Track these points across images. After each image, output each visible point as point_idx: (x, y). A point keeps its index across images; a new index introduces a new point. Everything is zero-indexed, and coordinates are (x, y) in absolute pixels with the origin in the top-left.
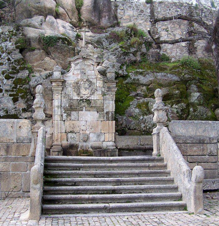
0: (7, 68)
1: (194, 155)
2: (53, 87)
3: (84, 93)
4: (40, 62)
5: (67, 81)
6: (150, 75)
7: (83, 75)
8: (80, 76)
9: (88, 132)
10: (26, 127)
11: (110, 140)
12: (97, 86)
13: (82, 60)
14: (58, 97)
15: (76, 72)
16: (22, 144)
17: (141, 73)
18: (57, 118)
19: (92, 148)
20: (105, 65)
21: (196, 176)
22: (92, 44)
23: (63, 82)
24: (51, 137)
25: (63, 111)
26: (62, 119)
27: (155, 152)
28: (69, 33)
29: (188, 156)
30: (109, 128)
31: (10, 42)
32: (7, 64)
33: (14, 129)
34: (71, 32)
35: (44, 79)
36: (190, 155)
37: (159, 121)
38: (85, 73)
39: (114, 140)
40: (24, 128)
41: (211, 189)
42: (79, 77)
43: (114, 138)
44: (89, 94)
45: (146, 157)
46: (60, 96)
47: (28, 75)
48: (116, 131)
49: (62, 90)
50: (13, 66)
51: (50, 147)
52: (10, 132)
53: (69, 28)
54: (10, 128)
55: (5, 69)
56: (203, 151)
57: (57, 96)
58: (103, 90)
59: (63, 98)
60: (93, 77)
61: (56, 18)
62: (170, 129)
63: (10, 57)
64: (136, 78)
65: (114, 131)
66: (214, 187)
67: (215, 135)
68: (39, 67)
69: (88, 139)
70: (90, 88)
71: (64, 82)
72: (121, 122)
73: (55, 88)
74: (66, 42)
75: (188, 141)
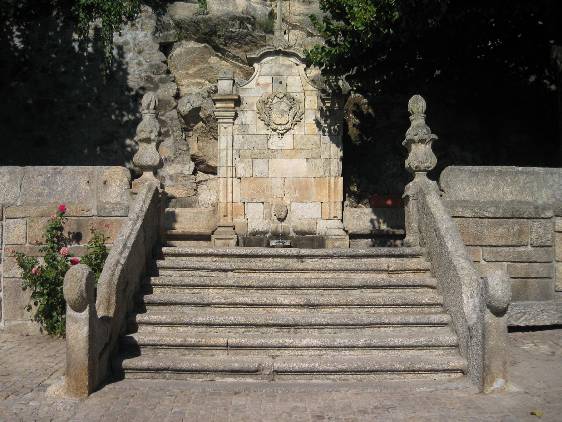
0: (136, 80)
2: (215, 111)
4: (201, 66)
5: (245, 99)
7: (277, 84)
8: (271, 87)
9: (287, 201)
10: (118, 183)
11: (332, 216)
12: (307, 106)
14: (226, 130)
16: (108, 218)
19: (295, 232)
22: (302, 29)
28: (255, 9)
30: (329, 192)
31: (143, 30)
32: (136, 73)
33: (92, 187)
35: (205, 98)
39: (340, 217)
40: (114, 185)
41: (537, 324)
42: (270, 90)
46: (230, 129)
54: (84, 186)
56: (520, 235)
57: (225, 128)
59: (236, 132)
63: (142, 59)
66: (544, 321)
67: (548, 199)
71: (238, 102)
74: (249, 26)
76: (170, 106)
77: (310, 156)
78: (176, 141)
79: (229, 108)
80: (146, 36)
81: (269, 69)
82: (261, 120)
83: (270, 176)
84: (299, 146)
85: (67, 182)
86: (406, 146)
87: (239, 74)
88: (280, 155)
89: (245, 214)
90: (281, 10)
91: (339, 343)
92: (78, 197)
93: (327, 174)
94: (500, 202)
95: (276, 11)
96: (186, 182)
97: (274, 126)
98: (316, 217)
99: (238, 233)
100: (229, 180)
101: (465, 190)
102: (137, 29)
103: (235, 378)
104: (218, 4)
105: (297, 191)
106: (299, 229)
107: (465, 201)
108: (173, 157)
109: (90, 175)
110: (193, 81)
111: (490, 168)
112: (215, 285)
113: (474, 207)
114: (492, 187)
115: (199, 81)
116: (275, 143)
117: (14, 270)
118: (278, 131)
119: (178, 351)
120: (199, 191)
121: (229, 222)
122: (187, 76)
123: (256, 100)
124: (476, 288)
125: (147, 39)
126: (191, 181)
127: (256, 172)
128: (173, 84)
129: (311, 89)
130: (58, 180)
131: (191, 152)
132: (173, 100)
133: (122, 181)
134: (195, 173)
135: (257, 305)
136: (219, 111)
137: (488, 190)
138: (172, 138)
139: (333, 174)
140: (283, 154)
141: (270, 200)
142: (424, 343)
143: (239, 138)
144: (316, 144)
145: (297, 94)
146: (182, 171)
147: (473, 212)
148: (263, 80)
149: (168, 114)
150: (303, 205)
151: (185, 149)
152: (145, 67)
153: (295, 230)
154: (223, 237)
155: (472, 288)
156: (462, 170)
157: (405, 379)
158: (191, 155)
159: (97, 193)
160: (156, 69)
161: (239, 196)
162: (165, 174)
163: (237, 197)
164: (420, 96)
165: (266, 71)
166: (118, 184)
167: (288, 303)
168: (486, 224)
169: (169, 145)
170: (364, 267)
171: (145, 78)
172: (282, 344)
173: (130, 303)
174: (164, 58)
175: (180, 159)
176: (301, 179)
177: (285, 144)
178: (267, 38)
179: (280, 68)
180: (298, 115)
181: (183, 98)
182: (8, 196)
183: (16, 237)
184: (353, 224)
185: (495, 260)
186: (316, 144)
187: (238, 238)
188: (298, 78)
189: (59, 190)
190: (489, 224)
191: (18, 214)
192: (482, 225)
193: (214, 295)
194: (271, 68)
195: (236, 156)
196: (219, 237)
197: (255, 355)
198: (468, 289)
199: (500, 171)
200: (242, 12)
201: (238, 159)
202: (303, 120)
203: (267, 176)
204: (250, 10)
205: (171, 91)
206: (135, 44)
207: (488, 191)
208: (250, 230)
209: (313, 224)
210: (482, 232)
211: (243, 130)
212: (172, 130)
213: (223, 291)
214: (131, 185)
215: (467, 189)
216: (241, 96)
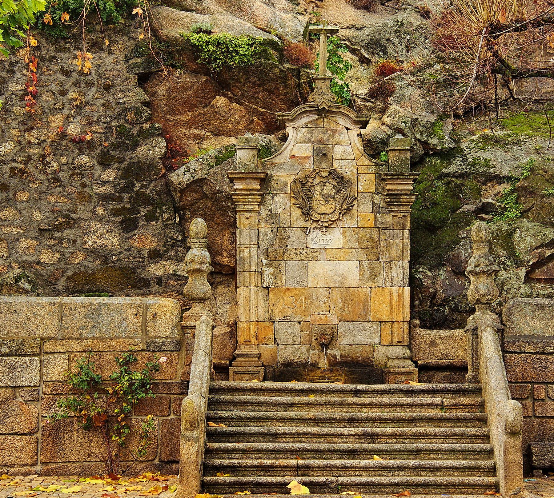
0: (102, 131)
3: (322, 209)
4: (200, 110)
6: (523, 147)
8: (311, 161)
11: (395, 340)
12: (360, 188)
17: (500, 143)
20: (389, 119)
21: (506, 421)
23: (262, 180)
24: (231, 332)
25: (265, 262)
26: (262, 283)
27: (469, 374)
31: (111, 53)
34: (288, 17)
37: (478, 300)
38: (325, 155)
40: (164, 318)
42: (309, 165)
43: (406, 336)
44: (337, 212)
47: (163, 151)
50: (119, 126)
51: (228, 362)
55: (225, 476)
59: (263, 225)
63: (110, 99)
64: (482, 155)
68: (198, 127)
72: (432, 290)
73: (241, 198)
75: (549, 348)
78: (165, 226)
79: (253, 190)
80: (116, 63)
82: (297, 207)
83: (309, 285)
85: (113, 315)
87: (259, 124)
88: (323, 257)
89: (275, 339)
97: (315, 217)
99: (265, 364)
102: (102, 50)
109: (138, 307)
110: (187, 132)
112: (278, 418)
115: (197, 131)
117: (54, 408)
123: (289, 180)
128: (161, 139)
129: (366, 164)
130: (103, 313)
135: (319, 435)
136: (239, 194)
139: (397, 282)
142: (466, 465)
143: (266, 232)
151: (180, 238)
171: (116, 130)
177: (330, 241)
179: (323, 133)
180: (349, 200)
182: (48, 330)
183: (57, 373)
189: (105, 322)
191: (59, 349)
192: (547, 360)
193: (275, 428)
194: (311, 132)
196: (240, 369)
202: (355, 207)
203: (306, 285)
206: (99, 74)
208: (281, 360)
211: (272, 221)
214: (181, 317)
215: (531, 323)
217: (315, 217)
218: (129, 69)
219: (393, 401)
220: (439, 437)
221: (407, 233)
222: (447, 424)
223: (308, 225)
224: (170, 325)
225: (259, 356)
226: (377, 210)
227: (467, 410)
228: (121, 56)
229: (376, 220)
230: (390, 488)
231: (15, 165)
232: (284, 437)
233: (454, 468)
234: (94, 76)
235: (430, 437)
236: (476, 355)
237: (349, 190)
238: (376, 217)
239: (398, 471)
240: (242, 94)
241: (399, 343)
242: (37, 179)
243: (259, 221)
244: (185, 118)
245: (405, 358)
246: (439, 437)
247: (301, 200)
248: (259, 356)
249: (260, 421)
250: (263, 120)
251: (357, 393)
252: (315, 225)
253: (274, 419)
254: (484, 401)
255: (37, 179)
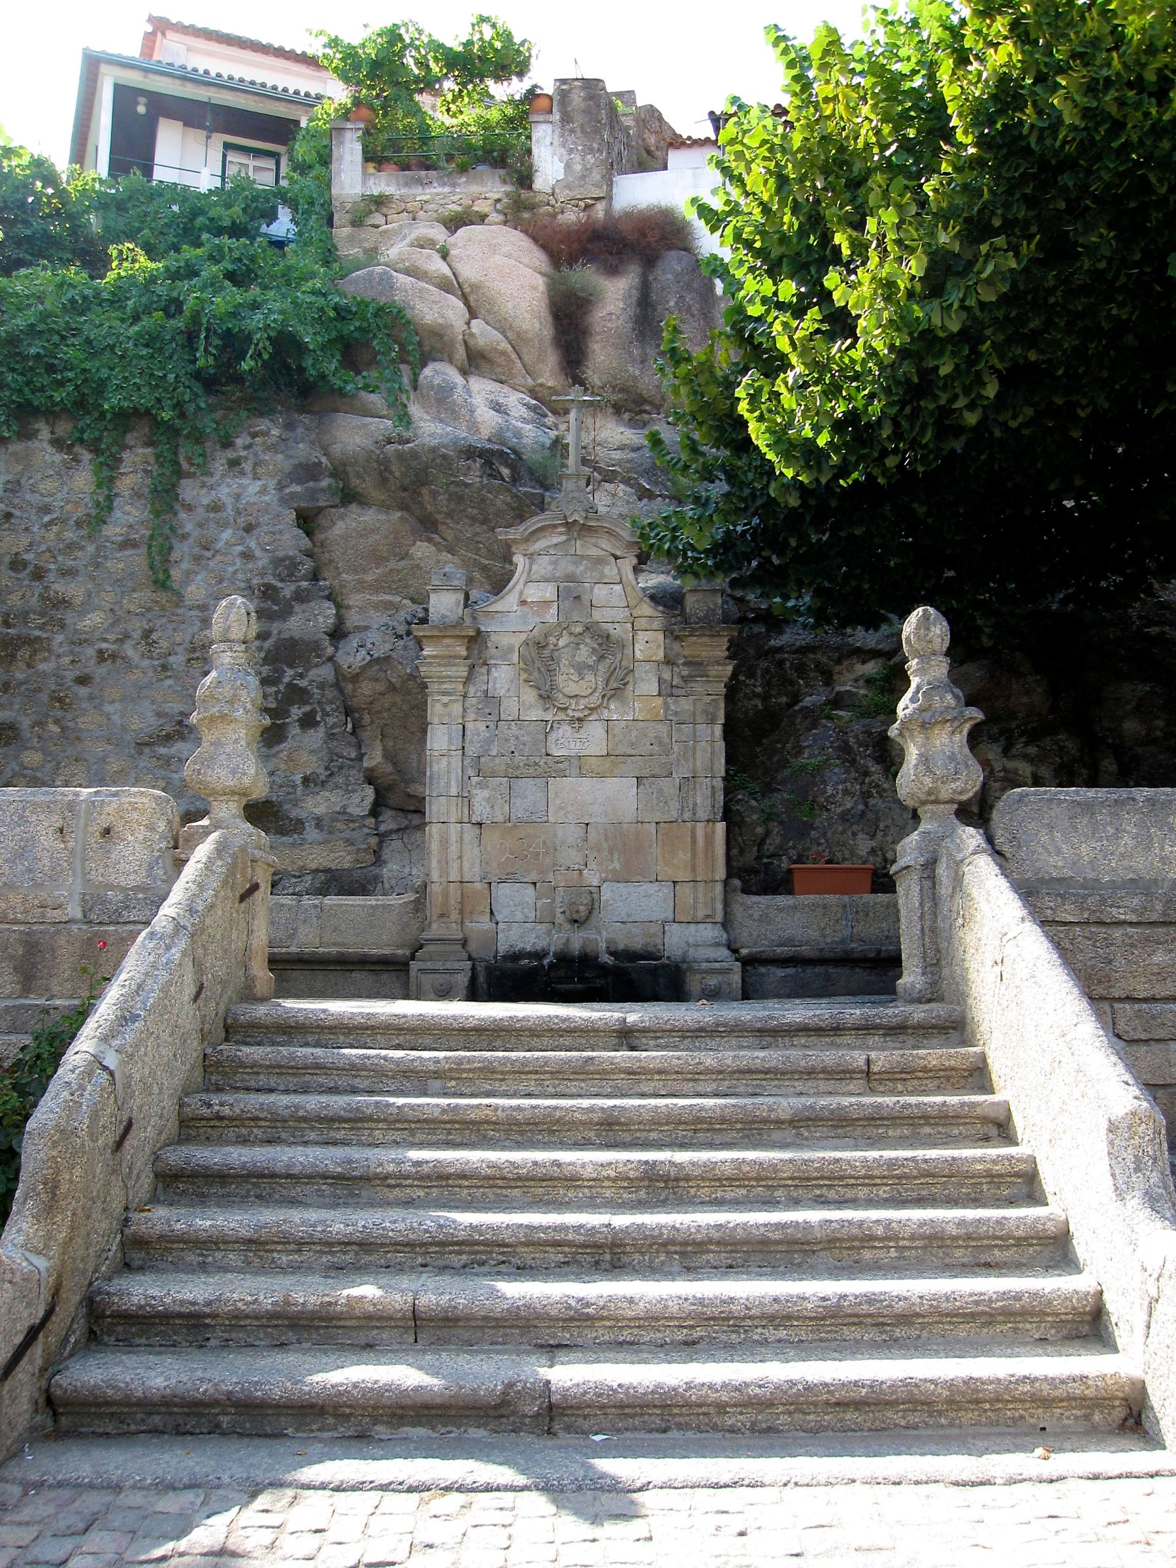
1: (1154, 999)
3: (572, 689)
4: (392, 564)
5: (494, 638)
7: (567, 604)
8: (553, 610)
11: (700, 914)
12: (638, 655)
13: (564, 538)
15: (534, 593)
18: (443, 809)
19: (611, 954)
22: (627, 481)
27: (911, 977)
28: (518, 434)
29: (1120, 1000)
30: (694, 857)
31: (256, 477)
32: (240, 576)
33: (71, 844)
35: (400, 637)
36: (1128, 999)
38: (578, 598)
39: (719, 917)
40: (130, 838)
43: (719, 906)
45: (854, 1012)
46: (457, 709)
47: (331, 621)
48: (732, 870)
49: (468, 681)
52: (46, 862)
53: (523, 411)
54: (47, 840)
58: (667, 675)
59: (471, 716)
60: (614, 612)
61: (464, 373)
62: (999, 840)
65: (721, 873)
68: (391, 591)
69: (595, 912)
70: (602, 668)
71: (477, 640)
74: (506, 472)
76: (318, 656)
77: (646, 773)
78: (331, 736)
80: (263, 491)
81: (551, 567)
83: (551, 819)
84: (621, 750)
86: (899, 740)
88: (575, 771)
89: (492, 912)
90: (578, 438)
91: (747, 1308)
92: (30, 871)
93: (687, 816)
94: (1155, 881)
95: (570, 439)
96: (355, 834)
97: (562, 700)
98: (662, 917)
99: (474, 955)
100: (454, 829)
101: (1059, 851)
102: (243, 473)
103: (433, 1429)
104: (434, 419)
105: (616, 855)
106: (621, 947)
107: (1061, 880)
108: (323, 774)
111: (1123, 793)
112: (391, 1118)
113: (1085, 897)
114: (1131, 843)
116: (564, 742)
118: (570, 712)
119: (266, 1333)
120: (386, 854)
121: (455, 932)
122: (362, 586)
123: (517, 641)
124: (1151, 1140)
125: (267, 498)
126: (366, 830)
127: (520, 809)
128: (327, 604)
131: (366, 764)
132: (326, 642)
133: (151, 828)
134: (374, 812)
137: (1122, 850)
138: (322, 729)
139: (702, 814)
140: (579, 765)
141: (550, 877)
144: (660, 743)
145: (616, 626)
146: (344, 807)
147: (1082, 909)
148: (534, 593)
149: (313, 673)
150: (631, 887)
151: (353, 755)
152: (260, 564)
153: (612, 949)
154: (439, 965)
155: (1137, 1140)
156: (1050, 800)
157: (951, 1425)
158: (367, 769)
159: (84, 860)
160: (286, 567)
161: (477, 869)
162: (303, 815)
163: (472, 870)
164: (931, 610)
165: (543, 572)
166: (141, 837)
167: (594, 1175)
168: (1118, 942)
169: (315, 746)
170: (803, 1063)
172: (576, 1311)
173: (138, 1177)
174: (305, 542)
175: (340, 780)
176: (625, 826)
178: (547, 500)
179: (575, 563)
180: (619, 673)
181: (351, 637)
184: (750, 934)
185: (1149, 1036)
186: (660, 743)
187: (473, 969)
188: (618, 588)
190: (1127, 941)
194: (555, 563)
195: (470, 772)
196: (429, 965)
197: (497, 1343)
198: (1124, 1143)
199: (1151, 802)
200: (489, 440)
201: (475, 780)
202: (630, 687)
204: (509, 434)
205: (321, 620)
207: (1122, 855)
208: (502, 949)
209: (654, 935)
210: (1110, 962)
212: (323, 710)
213: (413, 1136)
216: (483, 629)
217: (562, 700)
218: (284, 501)
219: (729, 1062)
220: (878, 1181)
221: (718, 730)
222: (890, 1133)
223: (549, 716)
224: (143, 854)
225: (464, 943)
226: (667, 691)
227: (936, 1082)
228: (272, 484)
229: (666, 707)
230: (741, 1413)
231: (104, 645)
232: (397, 1186)
233: (956, 1315)
234: (230, 511)
235: (852, 1181)
236: (933, 930)
237: (619, 656)
238: (666, 704)
239: (764, 1327)
240: (456, 538)
241: (708, 919)
242: (137, 667)
243: (464, 710)
244: (369, 578)
245: (717, 945)
246: (878, 1181)
247: (536, 674)
248: (464, 943)
249: (336, 1125)
250: (488, 577)
251: (626, 1037)
252: (561, 716)
253: (378, 1121)
254: (983, 1057)
255: (137, 667)
